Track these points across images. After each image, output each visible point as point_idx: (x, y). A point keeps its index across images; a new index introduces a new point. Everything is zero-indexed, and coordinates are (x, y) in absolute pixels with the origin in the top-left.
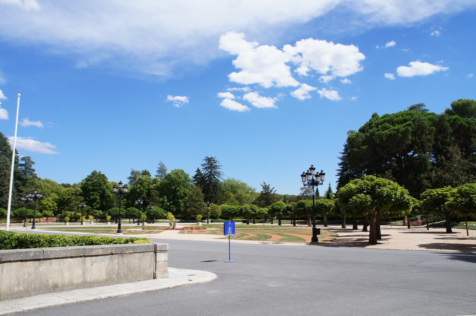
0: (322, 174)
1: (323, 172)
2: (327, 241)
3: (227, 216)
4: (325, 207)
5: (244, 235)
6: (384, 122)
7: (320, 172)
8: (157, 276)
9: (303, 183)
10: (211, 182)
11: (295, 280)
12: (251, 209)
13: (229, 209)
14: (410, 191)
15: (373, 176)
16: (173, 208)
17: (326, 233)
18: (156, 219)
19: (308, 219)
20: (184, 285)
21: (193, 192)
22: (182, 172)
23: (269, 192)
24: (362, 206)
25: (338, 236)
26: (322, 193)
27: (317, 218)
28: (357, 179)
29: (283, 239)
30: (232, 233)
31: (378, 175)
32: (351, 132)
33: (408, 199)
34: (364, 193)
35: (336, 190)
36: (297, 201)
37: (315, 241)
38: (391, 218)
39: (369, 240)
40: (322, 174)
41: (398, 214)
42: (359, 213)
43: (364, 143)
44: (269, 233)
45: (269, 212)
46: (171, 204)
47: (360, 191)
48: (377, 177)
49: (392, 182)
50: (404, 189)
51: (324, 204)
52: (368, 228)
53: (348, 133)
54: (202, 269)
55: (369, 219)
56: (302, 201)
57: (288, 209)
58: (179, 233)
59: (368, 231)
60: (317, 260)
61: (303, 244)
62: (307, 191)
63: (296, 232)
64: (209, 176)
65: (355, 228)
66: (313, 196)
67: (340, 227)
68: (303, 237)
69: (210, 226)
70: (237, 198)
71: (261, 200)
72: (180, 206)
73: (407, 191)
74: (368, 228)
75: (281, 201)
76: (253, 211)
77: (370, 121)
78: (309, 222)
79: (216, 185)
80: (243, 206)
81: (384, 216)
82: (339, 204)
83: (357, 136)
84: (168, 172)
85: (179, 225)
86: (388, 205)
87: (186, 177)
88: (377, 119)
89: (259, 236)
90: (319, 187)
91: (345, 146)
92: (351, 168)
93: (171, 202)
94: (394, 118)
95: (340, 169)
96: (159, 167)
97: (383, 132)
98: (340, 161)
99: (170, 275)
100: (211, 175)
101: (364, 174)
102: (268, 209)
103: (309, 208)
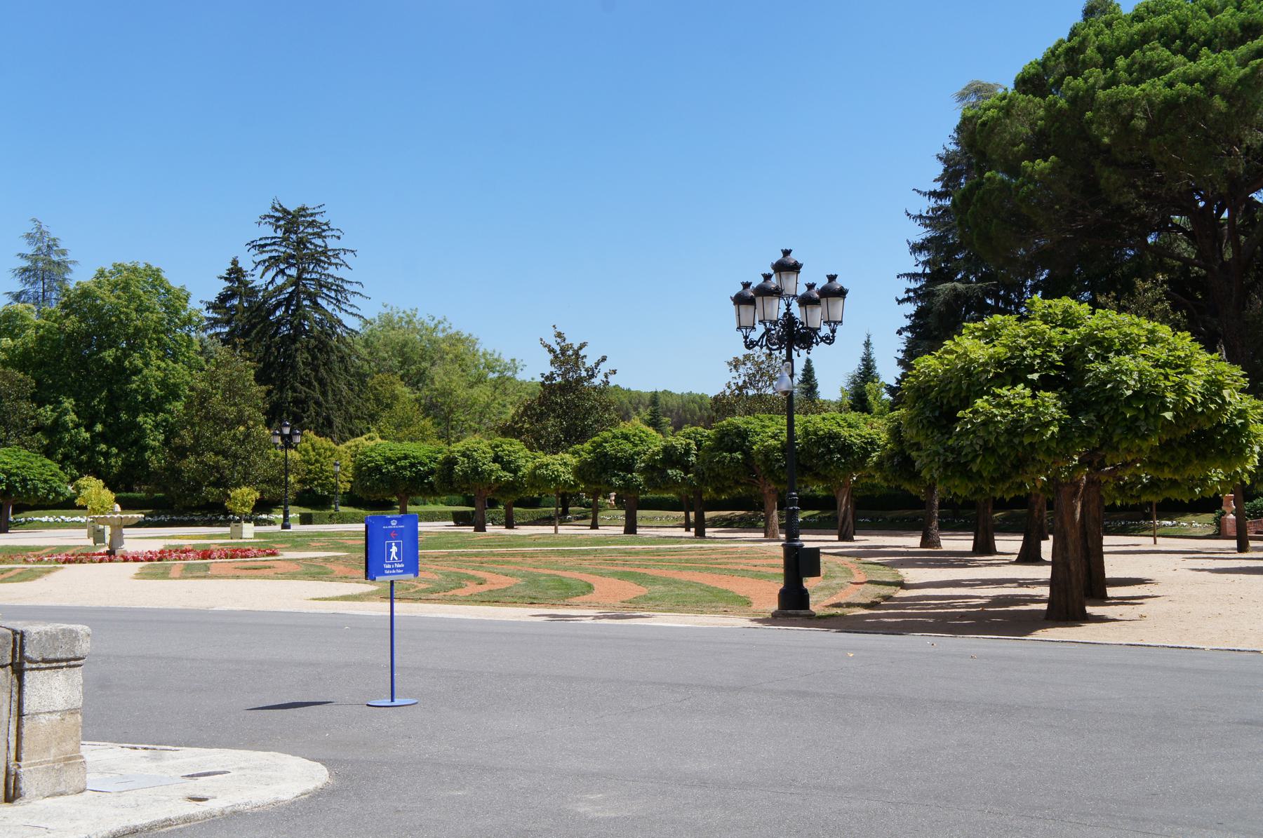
0: (833, 292)
1: (839, 283)
2: (849, 605)
3: (383, 492)
4: (846, 449)
5: (460, 581)
6: (1145, 37)
7: (821, 282)
8: (25, 785)
9: (740, 335)
10: (298, 330)
11: (703, 784)
12: (496, 459)
13: (389, 461)
14: (1251, 373)
15: (1073, 303)
16: (106, 455)
17: (849, 572)
18: (19, 509)
19: (761, 507)
20: (168, 822)
21: (212, 378)
22: (154, 278)
23: (580, 380)
24: (1016, 445)
25: (902, 585)
26: (832, 387)
27: (807, 503)
28: (998, 318)
29: (647, 599)
30: (405, 571)
31: (1101, 299)
32: (978, 90)
33: (1241, 413)
34: (1029, 384)
35: (899, 371)
36: (713, 420)
37: (794, 603)
38: (1155, 499)
39: (1050, 601)
40: (833, 292)
41: (1192, 483)
42: (1004, 477)
43: (1039, 145)
44: (580, 569)
45: (580, 471)
46: (97, 438)
47: (1012, 371)
48: (1095, 305)
49: (1164, 331)
50: (1224, 366)
51: (838, 436)
52: (1047, 548)
53: (962, 96)
54: (252, 743)
55: (1050, 505)
56: (738, 420)
57: (671, 457)
58: (141, 575)
59: (1044, 563)
60: (803, 694)
61: (740, 622)
62: (761, 374)
63: (710, 566)
64: (288, 301)
65: (984, 547)
66: (789, 395)
67: (912, 542)
68: (740, 586)
69: (299, 543)
70: (429, 409)
71: (541, 417)
72: (145, 448)
73: (1237, 371)
74: (1047, 548)
75: (636, 421)
76: (506, 466)
77: (1073, 33)
78: (767, 519)
79: (325, 346)
80: (459, 446)
81: (1121, 489)
82: (909, 434)
83: (1008, 109)
84: (80, 276)
85: (141, 540)
86: (1144, 437)
87: (174, 302)
88: (1109, 25)
89: (533, 581)
90: (819, 354)
91: (947, 159)
92: (972, 264)
93: (99, 428)
94: (1195, 16)
95: (920, 270)
96: (30, 250)
97: (1137, 91)
98: (920, 233)
99: (92, 779)
100: (299, 296)
101: (1033, 292)
102: (573, 461)
103: (768, 452)
